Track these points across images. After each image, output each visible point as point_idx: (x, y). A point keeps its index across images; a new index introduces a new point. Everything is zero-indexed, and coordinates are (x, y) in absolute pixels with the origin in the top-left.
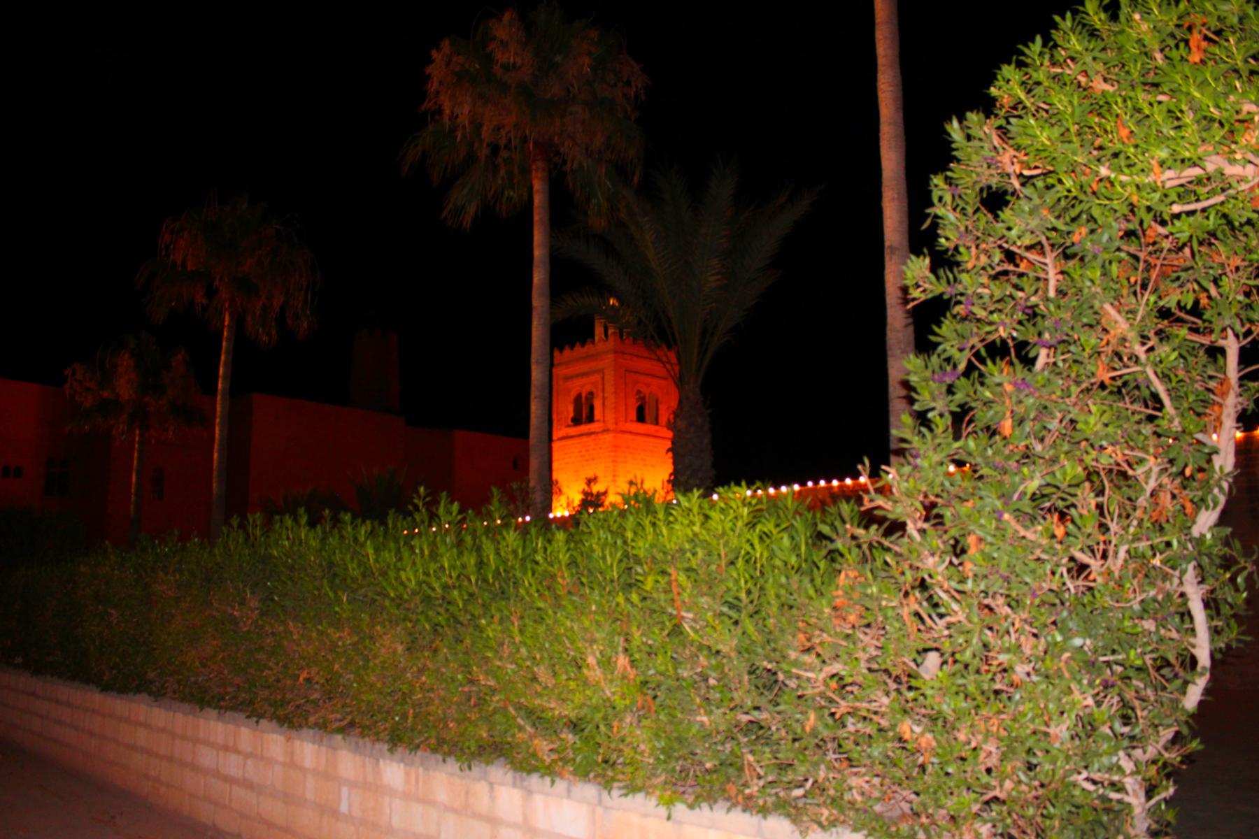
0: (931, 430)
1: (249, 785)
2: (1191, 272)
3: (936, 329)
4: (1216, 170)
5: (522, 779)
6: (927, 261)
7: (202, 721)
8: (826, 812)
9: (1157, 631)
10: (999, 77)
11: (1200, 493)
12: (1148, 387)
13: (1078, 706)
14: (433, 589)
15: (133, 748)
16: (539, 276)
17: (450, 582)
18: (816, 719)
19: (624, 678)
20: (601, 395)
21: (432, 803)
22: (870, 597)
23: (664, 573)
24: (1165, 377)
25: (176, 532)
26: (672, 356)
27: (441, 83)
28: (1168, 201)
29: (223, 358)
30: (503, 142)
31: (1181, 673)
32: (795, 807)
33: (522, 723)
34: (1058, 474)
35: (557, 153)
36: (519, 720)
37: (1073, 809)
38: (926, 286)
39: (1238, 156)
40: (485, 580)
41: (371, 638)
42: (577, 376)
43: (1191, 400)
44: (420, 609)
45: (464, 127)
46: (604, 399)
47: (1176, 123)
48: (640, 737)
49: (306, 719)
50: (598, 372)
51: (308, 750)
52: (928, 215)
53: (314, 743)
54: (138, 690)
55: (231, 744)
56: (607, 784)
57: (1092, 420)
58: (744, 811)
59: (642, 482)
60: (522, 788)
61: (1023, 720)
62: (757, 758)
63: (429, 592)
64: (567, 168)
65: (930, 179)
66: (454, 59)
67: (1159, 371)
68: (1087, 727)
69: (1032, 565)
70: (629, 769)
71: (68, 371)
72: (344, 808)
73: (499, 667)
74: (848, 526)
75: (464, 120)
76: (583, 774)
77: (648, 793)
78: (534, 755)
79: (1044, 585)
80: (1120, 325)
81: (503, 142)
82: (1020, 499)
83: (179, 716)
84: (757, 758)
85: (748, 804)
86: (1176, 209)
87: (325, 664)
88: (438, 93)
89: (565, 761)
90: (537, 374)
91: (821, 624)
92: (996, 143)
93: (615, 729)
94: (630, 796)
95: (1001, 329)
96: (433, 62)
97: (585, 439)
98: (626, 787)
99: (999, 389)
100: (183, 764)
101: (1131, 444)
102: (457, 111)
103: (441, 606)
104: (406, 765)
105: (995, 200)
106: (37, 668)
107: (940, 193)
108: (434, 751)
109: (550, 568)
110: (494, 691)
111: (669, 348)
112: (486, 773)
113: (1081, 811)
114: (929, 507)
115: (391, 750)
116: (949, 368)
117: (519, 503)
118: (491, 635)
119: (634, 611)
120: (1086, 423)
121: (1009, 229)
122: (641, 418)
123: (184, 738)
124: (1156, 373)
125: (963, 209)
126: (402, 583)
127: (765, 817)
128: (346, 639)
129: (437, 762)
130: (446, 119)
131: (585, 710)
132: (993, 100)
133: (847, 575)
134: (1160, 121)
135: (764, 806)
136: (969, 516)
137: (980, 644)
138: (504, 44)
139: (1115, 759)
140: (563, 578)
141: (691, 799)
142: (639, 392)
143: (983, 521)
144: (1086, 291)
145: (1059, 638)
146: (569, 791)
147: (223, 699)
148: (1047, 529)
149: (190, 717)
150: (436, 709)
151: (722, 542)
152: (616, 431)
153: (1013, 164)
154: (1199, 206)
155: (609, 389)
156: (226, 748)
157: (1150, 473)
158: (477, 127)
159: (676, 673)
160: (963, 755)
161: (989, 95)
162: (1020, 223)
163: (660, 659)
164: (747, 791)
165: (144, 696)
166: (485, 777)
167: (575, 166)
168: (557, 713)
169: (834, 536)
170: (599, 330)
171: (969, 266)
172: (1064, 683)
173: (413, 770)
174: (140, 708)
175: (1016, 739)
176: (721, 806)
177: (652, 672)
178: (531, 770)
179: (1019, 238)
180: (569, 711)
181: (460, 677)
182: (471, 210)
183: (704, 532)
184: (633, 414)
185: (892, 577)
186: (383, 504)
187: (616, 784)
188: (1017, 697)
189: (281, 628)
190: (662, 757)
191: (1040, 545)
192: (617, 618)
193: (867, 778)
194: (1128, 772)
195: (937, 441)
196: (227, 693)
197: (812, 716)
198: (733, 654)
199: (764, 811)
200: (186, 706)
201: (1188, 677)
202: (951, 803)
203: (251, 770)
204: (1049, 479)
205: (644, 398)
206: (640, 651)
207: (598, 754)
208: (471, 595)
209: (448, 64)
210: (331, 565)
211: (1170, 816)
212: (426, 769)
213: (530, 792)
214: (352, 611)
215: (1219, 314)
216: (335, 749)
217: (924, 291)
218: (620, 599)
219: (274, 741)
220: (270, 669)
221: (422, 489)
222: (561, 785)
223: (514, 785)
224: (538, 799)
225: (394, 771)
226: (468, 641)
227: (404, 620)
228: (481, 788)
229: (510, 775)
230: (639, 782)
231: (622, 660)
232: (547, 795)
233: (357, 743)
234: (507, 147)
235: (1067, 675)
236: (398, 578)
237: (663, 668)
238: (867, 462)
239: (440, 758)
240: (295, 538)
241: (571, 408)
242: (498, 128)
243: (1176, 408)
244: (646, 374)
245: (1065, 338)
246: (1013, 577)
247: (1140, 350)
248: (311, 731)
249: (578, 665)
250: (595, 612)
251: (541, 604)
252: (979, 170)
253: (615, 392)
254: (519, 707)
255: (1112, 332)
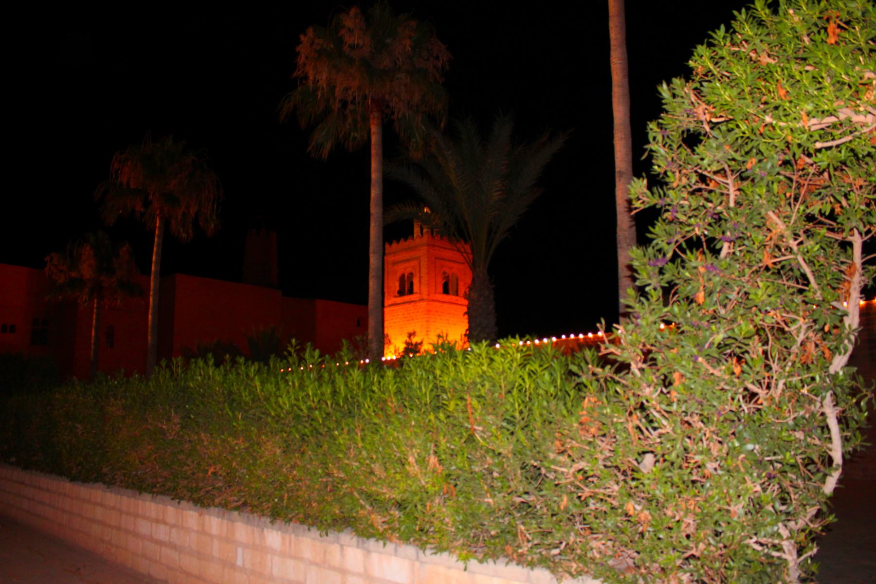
0: (648, 299)
1: (173, 546)
2: (828, 189)
3: (651, 229)
4: (846, 119)
5: (363, 543)
6: (645, 181)
7: (140, 502)
8: (574, 565)
9: (805, 439)
10: (695, 54)
11: (835, 343)
12: (799, 269)
13: (750, 492)
14: (301, 410)
15: (93, 520)
16: (375, 192)
17: (313, 405)
18: (568, 501)
19: (434, 472)
20: (418, 275)
21: (301, 559)
22: (605, 415)
23: (462, 399)
24: (810, 263)
25: (123, 371)
26: (468, 248)
27: (307, 58)
28: (813, 140)
29: (155, 249)
30: (350, 99)
31: (822, 468)
32: (553, 562)
33: (363, 503)
34: (736, 330)
35: (388, 107)
36: (361, 501)
37: (747, 563)
38: (645, 199)
39: (861, 109)
40: (338, 404)
41: (258, 444)
42: (402, 262)
43: (828, 278)
44: (292, 424)
45: (323, 88)
46: (420, 277)
47: (818, 86)
48: (445, 513)
49: (213, 501)
50: (416, 259)
51: (214, 522)
52: (646, 150)
53: (218, 517)
54: (96, 481)
55: (161, 518)
56: (423, 546)
57: (760, 292)
58: (518, 564)
59: (447, 336)
60: (363, 548)
61: (712, 501)
62: (527, 527)
63: (299, 412)
64: (395, 117)
65: (647, 125)
66: (316, 41)
67: (806, 258)
68: (757, 506)
69: (718, 393)
70: (438, 536)
71: (47, 258)
72: (239, 562)
73: (347, 464)
74: (590, 366)
75: (323, 83)
76: (406, 539)
77: (451, 552)
78: (372, 526)
79: (726, 407)
80: (779, 226)
81: (350, 99)
82: (709, 347)
83: (125, 498)
84: (527, 527)
85: (521, 560)
86: (818, 145)
87: (226, 462)
88: (305, 65)
89: (393, 530)
90: (374, 261)
91: (571, 435)
92: (693, 100)
93: (428, 508)
94: (439, 554)
95: (696, 229)
96: (301, 43)
97: (407, 305)
98: (436, 548)
99: (695, 271)
100: (127, 532)
101: (787, 309)
102: (318, 77)
103: (307, 422)
104: (283, 532)
105: (692, 140)
106: (26, 465)
107: (654, 134)
108: (302, 523)
109: (383, 396)
110: (343, 481)
111: (466, 242)
112: (338, 538)
113: (752, 565)
114: (647, 353)
115: (272, 522)
116: (660, 256)
117: (361, 350)
118: (342, 442)
119: (441, 426)
120: (756, 294)
121: (702, 159)
122: (446, 291)
123: (128, 514)
124: (804, 260)
125: (670, 145)
126: (280, 406)
127: (532, 569)
128: (241, 445)
129: (304, 530)
130: (310, 83)
131: (407, 494)
132: (691, 70)
133: (589, 400)
134: (807, 84)
135: (531, 561)
136: (674, 359)
137: (682, 449)
138: (351, 31)
139: (775, 528)
140: (392, 402)
141: (481, 556)
142: (444, 273)
143: (684, 363)
144: (755, 202)
145: (737, 444)
146: (396, 550)
147: (155, 486)
148: (728, 368)
149: (133, 499)
150: (304, 494)
151: (502, 377)
152: (428, 300)
153: (705, 114)
154: (834, 143)
155: (424, 270)
156: (157, 521)
157: (800, 329)
158: (332, 88)
159: (471, 469)
160: (670, 525)
161: (688, 66)
162: (710, 156)
163: (459, 459)
164: (520, 551)
165: (100, 484)
166: (337, 541)
167: (400, 115)
168: (387, 496)
169: (580, 373)
170: (417, 230)
171: (675, 185)
172: (740, 475)
173: (287, 536)
174: (98, 493)
175: (707, 515)
176: (502, 561)
177: (453, 468)
178: (370, 536)
179: (709, 165)
180: (396, 495)
181: (320, 471)
182: (328, 146)
183: (490, 370)
184: (440, 289)
185: (621, 402)
186: (266, 351)
187: (428, 546)
188: (708, 485)
189: (196, 437)
190: (461, 527)
191: (724, 380)
192: (430, 430)
193: (603, 542)
194: (785, 537)
195: (652, 307)
196: (158, 483)
197: (565, 498)
198: (510, 456)
199: (532, 565)
200: (130, 491)
201: (827, 471)
202: (662, 559)
203: (175, 536)
204: (730, 333)
205: (448, 277)
206: (446, 453)
207: (416, 525)
208: (328, 414)
209: (312, 44)
210: (230, 393)
211: (814, 568)
212: (297, 535)
213: (369, 552)
214: (245, 425)
215: (848, 219)
216: (233, 521)
217: (643, 202)
218: (432, 417)
219: (191, 516)
220: (188, 465)
221: (293, 341)
222: (390, 546)
223: (358, 547)
224: (375, 556)
225: (274, 537)
226: (325, 446)
227: (281, 431)
228: (335, 548)
229: (355, 539)
230: (445, 544)
231: (433, 460)
232: (381, 553)
233: (248, 517)
234: (353, 102)
235: (742, 470)
236: (277, 402)
237: (461, 465)
238: (603, 321)
239: (306, 527)
240: (205, 374)
241: (397, 284)
242: (347, 89)
243: (819, 284)
244: (450, 261)
245: (741, 235)
246: (705, 401)
247: (793, 244)
248: (217, 509)
249: (402, 463)
250: (414, 426)
251: (376, 421)
252: (681, 118)
253: (428, 273)
254: (361, 492)
255: (774, 231)
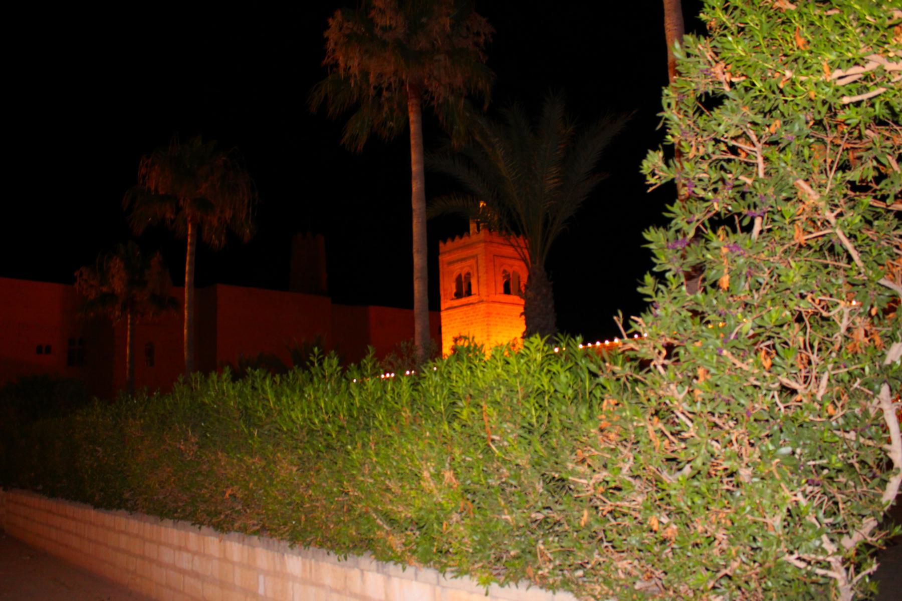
0: (667, 286)
1: (196, 575)
2: (870, 151)
3: (669, 207)
4: (878, 67)
5: (383, 567)
6: (661, 154)
7: (163, 528)
8: (599, 588)
9: (857, 440)
10: (706, 5)
11: (891, 329)
12: (841, 245)
13: (788, 501)
14: (314, 424)
15: (117, 549)
16: (417, 186)
17: (326, 418)
18: (590, 515)
19: (451, 487)
20: (476, 275)
21: (321, 586)
22: (625, 419)
23: (478, 406)
24: (852, 237)
25: (146, 389)
26: (521, 241)
27: (336, 44)
28: (839, 94)
29: (188, 258)
30: (385, 86)
31: (878, 473)
32: (577, 584)
33: (381, 523)
34: (766, 318)
35: (427, 92)
36: (378, 521)
37: (787, 583)
38: (661, 174)
39: (891, 54)
40: (351, 416)
41: (275, 463)
42: (458, 261)
43: (874, 254)
44: (306, 439)
45: (355, 76)
46: (478, 277)
47: (841, 31)
48: (459, 530)
49: (233, 525)
50: (473, 257)
51: (235, 548)
52: (661, 118)
53: (239, 542)
54: (119, 507)
55: (183, 545)
56: (442, 569)
57: (791, 274)
58: (541, 588)
59: (473, 338)
60: (383, 573)
61: (744, 513)
62: (547, 547)
63: (313, 427)
64: (434, 103)
65: (661, 90)
66: (345, 25)
67: (846, 231)
68: (793, 516)
69: (750, 391)
70: (457, 557)
71: (77, 274)
72: (261, 591)
73: (362, 481)
74: (607, 364)
75: (355, 71)
76: (425, 561)
77: (471, 575)
78: (390, 548)
79: (756, 405)
80: (811, 196)
81: (385, 86)
82: (736, 338)
83: (148, 526)
84: (547, 547)
85: (544, 583)
86: (846, 100)
87: (243, 483)
88: (334, 50)
89: (414, 552)
90: (419, 260)
91: (590, 441)
92: (709, 58)
93: (444, 526)
94: (459, 578)
95: (715, 205)
96: (329, 27)
97: (465, 308)
98: (457, 571)
99: (717, 251)
100: (151, 561)
101: (824, 291)
102: (350, 63)
103: (320, 436)
104: (303, 557)
105: (711, 102)
106: (52, 493)
107: (668, 101)
108: (321, 546)
109: (396, 406)
110: (360, 500)
111: (518, 235)
112: (358, 562)
113: (792, 584)
114: (669, 347)
115: (291, 546)
116: (680, 237)
117: (405, 358)
118: (355, 457)
119: (456, 437)
120: (787, 276)
121: (719, 125)
122: (507, 291)
123: (151, 541)
124: (844, 234)
125: (686, 111)
126: (293, 421)
127: (554, 593)
128: (257, 463)
129: (324, 554)
130: (342, 72)
131: (422, 513)
132: (703, 24)
133: (608, 403)
134: (829, 30)
135: (553, 584)
136: (697, 353)
137: (708, 455)
138: (382, 12)
139: (818, 543)
140: (405, 412)
141: (502, 578)
142: (504, 271)
143: (707, 357)
144: (781, 171)
145: (771, 447)
146: (416, 575)
147: (177, 512)
148: (756, 361)
149: (155, 526)
150: (320, 514)
151: (518, 380)
152: (488, 302)
153: (724, 73)
154: (865, 97)
155: (482, 269)
156: (180, 548)
157: (844, 312)
158: (365, 74)
159: (487, 483)
160: (698, 541)
161: (700, 19)
162: (726, 121)
163: (475, 473)
164: (540, 572)
165: (123, 511)
166: (357, 565)
167: (441, 101)
168: (403, 515)
169: (600, 373)
170: (473, 226)
171: (691, 156)
172: (775, 483)
173: (307, 561)
174: (119, 520)
175: (739, 528)
176: (523, 584)
177: (469, 482)
178: (390, 559)
179: (726, 132)
180: (411, 513)
181: (335, 489)
182: (364, 138)
183: (504, 374)
184: (501, 289)
185: (641, 403)
186: (286, 361)
187: (448, 569)
188: (738, 494)
189: (213, 457)
190: (478, 547)
191: (753, 374)
192: (447, 442)
193: (630, 561)
194: (830, 552)
195: (673, 295)
196: (179, 507)
197: (585, 513)
198: (528, 467)
199: (553, 588)
200: (152, 518)
201: (884, 477)
202: (692, 581)
203: (198, 564)
204: (758, 322)
205: (509, 275)
206: (461, 466)
207: (434, 546)
208: (342, 427)
209: (341, 29)
210: (246, 408)
211: (873, 588)
212: (317, 561)
213: (389, 576)
214: (261, 443)
215: (892, 183)
216: (253, 547)
217: (659, 178)
218: (446, 427)
219: (212, 543)
220: (206, 488)
221: (316, 350)
222: (410, 570)
223: (378, 571)
224: (395, 581)
225: (295, 563)
226: (340, 463)
227: (296, 448)
228: (356, 573)
229: (374, 563)
230: (465, 567)
231: (448, 475)
232: (401, 578)
233: (268, 542)
234: (388, 89)
235: (777, 476)
236: (290, 417)
237: (476, 479)
238: (620, 314)
239: (325, 551)
240: (221, 390)
241: (454, 286)
242: (381, 75)
243: (864, 262)
244: (511, 258)
245: (770, 209)
246: (733, 401)
247: (831, 217)
248: (237, 534)
249: (418, 477)
250: (429, 438)
251: (390, 433)
252: (696, 80)
253: (487, 273)
254: (376, 510)
255: (807, 203)
